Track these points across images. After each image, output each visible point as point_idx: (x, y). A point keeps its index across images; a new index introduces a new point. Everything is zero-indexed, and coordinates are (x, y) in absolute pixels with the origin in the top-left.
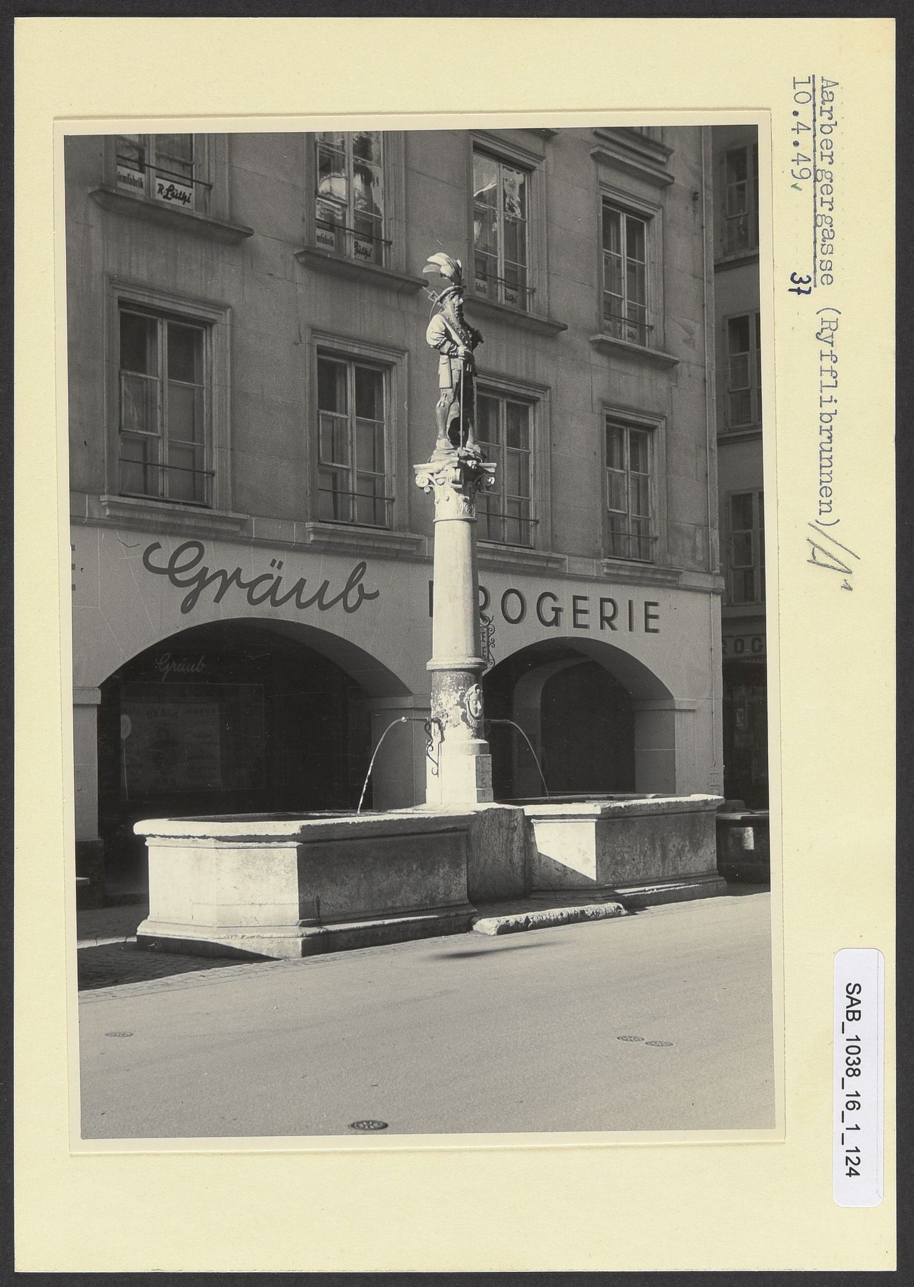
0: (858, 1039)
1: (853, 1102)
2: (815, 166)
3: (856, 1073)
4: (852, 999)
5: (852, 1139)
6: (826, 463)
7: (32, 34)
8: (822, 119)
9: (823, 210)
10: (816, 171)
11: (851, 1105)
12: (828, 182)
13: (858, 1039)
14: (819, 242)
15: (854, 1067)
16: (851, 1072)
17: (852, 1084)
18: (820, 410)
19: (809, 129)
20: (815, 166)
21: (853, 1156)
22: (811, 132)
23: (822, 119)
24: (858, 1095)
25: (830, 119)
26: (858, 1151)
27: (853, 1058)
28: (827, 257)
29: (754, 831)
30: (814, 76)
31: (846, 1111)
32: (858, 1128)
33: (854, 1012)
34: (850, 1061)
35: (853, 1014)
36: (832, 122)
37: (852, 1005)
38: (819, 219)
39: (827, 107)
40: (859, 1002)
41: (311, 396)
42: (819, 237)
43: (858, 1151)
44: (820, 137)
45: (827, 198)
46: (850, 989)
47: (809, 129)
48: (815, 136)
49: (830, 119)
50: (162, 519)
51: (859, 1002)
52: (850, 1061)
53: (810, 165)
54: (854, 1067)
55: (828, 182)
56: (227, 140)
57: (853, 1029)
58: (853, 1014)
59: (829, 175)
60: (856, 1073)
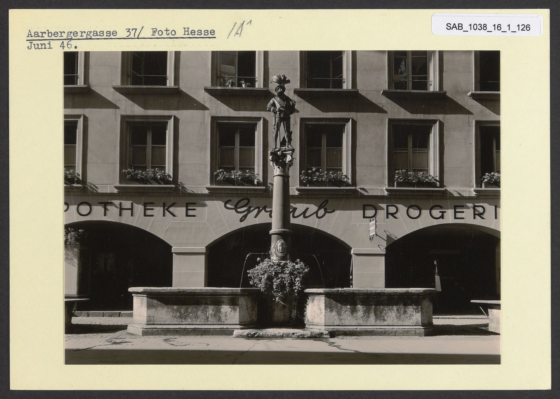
0: (471, 25)
1: (68, 45)
2: (65, 39)
3: (485, 26)
4: (453, 27)
5: (514, 28)
6: (43, 46)
7: (19, 381)
8: (46, 36)
9: (85, 36)
10: (68, 39)
11: (499, 28)
12: (72, 34)
13: (471, 25)
14: (99, 37)
15: (482, 27)
16: (485, 28)
17: (490, 27)
18: (78, 32)
19: (63, 42)
20: (65, 39)
21: (521, 28)
24: (495, 25)
25: (45, 33)
27: (478, 27)
28: (79, 34)
29: (282, 244)
30: (215, 37)
31: (502, 30)
33: (459, 26)
34: (480, 28)
35: (460, 27)
36: (47, 32)
37: (456, 27)
38: (88, 37)
39: (40, 34)
40: (454, 24)
42: (96, 37)
44: (53, 37)
45: (79, 34)
46: (449, 28)
47: (63, 42)
48: (53, 40)
49: (45, 33)
50: (216, 62)
51: (454, 24)
52: (480, 28)
53: (66, 42)
54: (482, 27)
55: (72, 34)
56: (143, 165)
58: (460, 27)
59: (69, 33)
60: (485, 26)
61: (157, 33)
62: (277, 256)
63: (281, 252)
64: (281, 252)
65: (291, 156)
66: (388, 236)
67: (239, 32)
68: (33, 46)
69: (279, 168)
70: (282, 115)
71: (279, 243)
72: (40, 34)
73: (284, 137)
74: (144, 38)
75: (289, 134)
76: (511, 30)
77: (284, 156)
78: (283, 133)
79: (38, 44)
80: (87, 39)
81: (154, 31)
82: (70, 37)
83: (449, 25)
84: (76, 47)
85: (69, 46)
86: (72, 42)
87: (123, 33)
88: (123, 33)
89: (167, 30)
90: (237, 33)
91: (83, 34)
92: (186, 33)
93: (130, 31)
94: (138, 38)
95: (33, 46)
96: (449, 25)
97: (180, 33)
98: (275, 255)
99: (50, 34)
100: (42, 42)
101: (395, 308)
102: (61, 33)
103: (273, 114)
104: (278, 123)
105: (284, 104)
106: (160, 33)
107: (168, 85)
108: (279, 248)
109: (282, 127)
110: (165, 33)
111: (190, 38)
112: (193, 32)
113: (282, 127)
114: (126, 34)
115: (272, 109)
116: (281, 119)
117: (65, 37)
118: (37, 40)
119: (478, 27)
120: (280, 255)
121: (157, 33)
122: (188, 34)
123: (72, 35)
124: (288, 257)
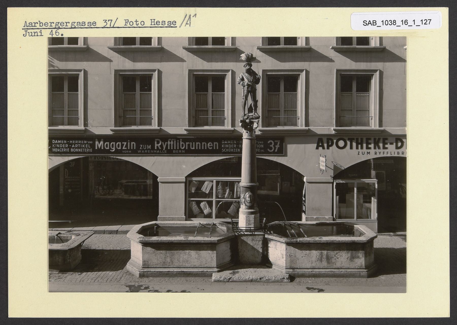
0: (383, 21)
2: (54, 28)
3: (395, 21)
5: (418, 22)
6: (36, 34)
7: (15, 310)
8: (38, 26)
10: (55, 28)
11: (406, 23)
13: (383, 21)
15: (392, 22)
16: (394, 23)
17: (399, 23)
20: (54, 28)
21: (424, 22)
22: (53, 29)
23: (38, 26)
24: (402, 21)
25: (37, 23)
26: (422, 20)
27: (389, 23)
28: (166, 23)
29: (250, 197)
31: (408, 25)
32: (414, 20)
34: (391, 24)
36: (39, 22)
37: (371, 23)
38: (57, 27)
41: (195, 156)
43: (422, 20)
44: (44, 27)
46: (365, 24)
49: (37, 23)
52: (391, 24)
53: (54, 31)
54: (392, 22)
57: (379, 23)
59: (73, 23)
60: (395, 21)
61: (128, 23)
62: (246, 205)
63: (249, 203)
64: (249, 203)
65: (257, 123)
66: (335, 166)
67: (189, 23)
68: (28, 34)
69: (247, 132)
70: (249, 90)
71: (247, 195)
72: (33, 25)
73: (251, 104)
74: (118, 27)
75: (255, 101)
76: (416, 24)
77: (252, 123)
78: (250, 101)
79: (31, 33)
80: (72, 28)
81: (127, 21)
82: (58, 27)
83: (365, 22)
84: (62, 35)
85: (57, 34)
86: (60, 31)
87: (100, 23)
88: (100, 23)
89: (136, 21)
90: (187, 24)
91: (52, 24)
92: (153, 23)
93: (107, 21)
94: (113, 27)
95: (28, 34)
96: (365, 22)
97: (148, 24)
98: (244, 204)
99: (41, 25)
100: (35, 31)
101: (350, 251)
102: (67, 23)
103: (242, 87)
104: (246, 95)
105: (251, 79)
106: (131, 23)
107: (226, 45)
108: (248, 199)
109: (249, 97)
110: (135, 23)
111: (81, 28)
112: (158, 22)
113: (249, 97)
114: (104, 24)
115: (241, 83)
116: (248, 92)
117: (54, 27)
118: (30, 28)
119: (389, 23)
120: (248, 204)
121: (128, 23)
122: (154, 25)
123: (59, 25)
124: (255, 205)
